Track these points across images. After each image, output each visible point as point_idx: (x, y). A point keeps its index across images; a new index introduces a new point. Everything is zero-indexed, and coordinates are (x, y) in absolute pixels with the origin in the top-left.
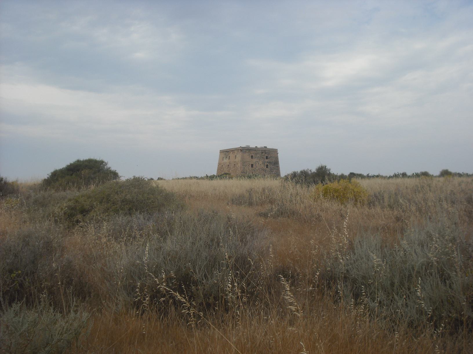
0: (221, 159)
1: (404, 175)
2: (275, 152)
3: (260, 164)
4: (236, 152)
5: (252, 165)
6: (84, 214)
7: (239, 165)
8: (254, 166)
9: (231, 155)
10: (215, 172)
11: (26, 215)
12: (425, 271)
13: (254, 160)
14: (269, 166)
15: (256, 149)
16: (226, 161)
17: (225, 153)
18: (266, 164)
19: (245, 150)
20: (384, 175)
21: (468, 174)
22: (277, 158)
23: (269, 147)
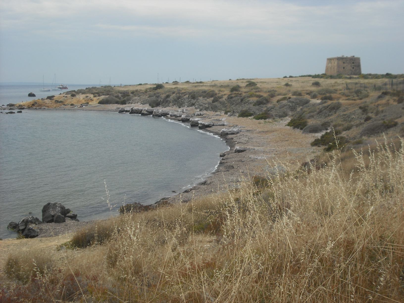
0: (328, 63)
1: (141, 84)
2: (358, 59)
3: (349, 67)
4: (335, 60)
5: (344, 68)
6: (397, 254)
7: (336, 67)
8: (345, 68)
9: (332, 61)
10: (322, 71)
11: (104, 244)
12: (332, 282)
13: (345, 65)
14: (354, 68)
15: (346, 59)
16: (330, 65)
17: (330, 60)
18: (353, 66)
19: (339, 59)
20: (133, 84)
21: (376, 86)
22: (359, 63)
23: (356, 56)
